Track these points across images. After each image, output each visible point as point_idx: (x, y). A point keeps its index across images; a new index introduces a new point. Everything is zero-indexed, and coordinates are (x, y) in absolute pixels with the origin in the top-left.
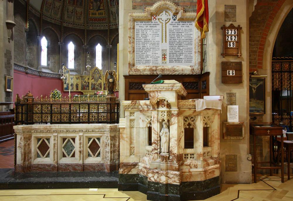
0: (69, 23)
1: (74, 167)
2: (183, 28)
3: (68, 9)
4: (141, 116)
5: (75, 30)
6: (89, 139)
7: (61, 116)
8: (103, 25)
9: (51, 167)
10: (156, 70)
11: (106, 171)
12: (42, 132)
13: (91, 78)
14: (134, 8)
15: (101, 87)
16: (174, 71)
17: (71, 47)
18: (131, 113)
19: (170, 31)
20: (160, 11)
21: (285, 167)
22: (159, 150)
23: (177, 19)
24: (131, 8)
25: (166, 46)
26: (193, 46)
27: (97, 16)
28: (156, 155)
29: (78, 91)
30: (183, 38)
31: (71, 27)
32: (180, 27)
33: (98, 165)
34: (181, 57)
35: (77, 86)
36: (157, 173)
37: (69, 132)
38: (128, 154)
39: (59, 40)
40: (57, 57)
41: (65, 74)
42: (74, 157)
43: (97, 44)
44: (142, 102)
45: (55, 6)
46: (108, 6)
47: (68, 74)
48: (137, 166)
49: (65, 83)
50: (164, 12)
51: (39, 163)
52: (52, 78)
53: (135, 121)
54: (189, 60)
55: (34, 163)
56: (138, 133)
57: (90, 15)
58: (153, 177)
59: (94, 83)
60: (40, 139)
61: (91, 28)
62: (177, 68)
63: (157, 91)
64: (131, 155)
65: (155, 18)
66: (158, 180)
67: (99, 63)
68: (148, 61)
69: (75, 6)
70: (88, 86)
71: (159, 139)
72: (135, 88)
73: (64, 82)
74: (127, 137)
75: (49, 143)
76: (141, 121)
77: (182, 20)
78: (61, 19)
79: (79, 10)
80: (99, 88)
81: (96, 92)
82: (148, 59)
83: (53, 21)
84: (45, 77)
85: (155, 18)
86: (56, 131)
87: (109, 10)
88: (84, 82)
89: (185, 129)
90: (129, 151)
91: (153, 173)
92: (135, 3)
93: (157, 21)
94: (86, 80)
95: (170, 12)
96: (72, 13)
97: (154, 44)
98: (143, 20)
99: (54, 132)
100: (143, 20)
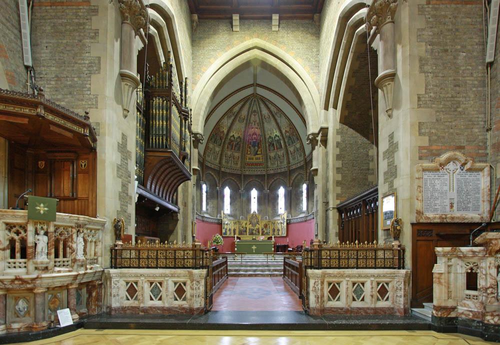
0: (227, 168)
1: (365, 310)
2: (471, 178)
3: (291, 151)
4: (460, 262)
5: (233, 175)
6: (378, 284)
9: (344, 310)
10: (446, 218)
11: (398, 314)
12: (335, 276)
13: (248, 223)
14: (420, 158)
15: (259, 232)
16: (464, 219)
17: (227, 191)
18: (448, 259)
19: (458, 180)
20: (448, 161)
22: (496, 294)
23: (465, 169)
25: (454, 194)
26: (481, 195)
30: (471, 187)
32: (467, 177)
33: (389, 309)
34: (469, 205)
35: (234, 231)
37: (174, 276)
38: (447, 299)
39: (218, 185)
40: (215, 202)
46: (266, 151)
48: (456, 310)
50: (452, 163)
51: (332, 307)
52: (212, 223)
54: (476, 208)
55: (327, 306)
56: (456, 279)
58: (493, 319)
60: (153, 283)
61: (247, 173)
62: (467, 216)
65: (443, 168)
67: (254, 207)
68: (436, 210)
69: (233, 151)
70: (246, 231)
71: (496, 283)
75: (339, 287)
76: (458, 267)
77: (470, 170)
79: (236, 155)
80: (257, 233)
81: (254, 237)
82: (436, 207)
83: (213, 166)
84: (207, 222)
85: (443, 168)
89: (467, 273)
90: (447, 295)
91: (492, 315)
94: (244, 225)
96: (230, 158)
97: (442, 193)
98: (432, 170)
99: (346, 277)
100: (432, 170)
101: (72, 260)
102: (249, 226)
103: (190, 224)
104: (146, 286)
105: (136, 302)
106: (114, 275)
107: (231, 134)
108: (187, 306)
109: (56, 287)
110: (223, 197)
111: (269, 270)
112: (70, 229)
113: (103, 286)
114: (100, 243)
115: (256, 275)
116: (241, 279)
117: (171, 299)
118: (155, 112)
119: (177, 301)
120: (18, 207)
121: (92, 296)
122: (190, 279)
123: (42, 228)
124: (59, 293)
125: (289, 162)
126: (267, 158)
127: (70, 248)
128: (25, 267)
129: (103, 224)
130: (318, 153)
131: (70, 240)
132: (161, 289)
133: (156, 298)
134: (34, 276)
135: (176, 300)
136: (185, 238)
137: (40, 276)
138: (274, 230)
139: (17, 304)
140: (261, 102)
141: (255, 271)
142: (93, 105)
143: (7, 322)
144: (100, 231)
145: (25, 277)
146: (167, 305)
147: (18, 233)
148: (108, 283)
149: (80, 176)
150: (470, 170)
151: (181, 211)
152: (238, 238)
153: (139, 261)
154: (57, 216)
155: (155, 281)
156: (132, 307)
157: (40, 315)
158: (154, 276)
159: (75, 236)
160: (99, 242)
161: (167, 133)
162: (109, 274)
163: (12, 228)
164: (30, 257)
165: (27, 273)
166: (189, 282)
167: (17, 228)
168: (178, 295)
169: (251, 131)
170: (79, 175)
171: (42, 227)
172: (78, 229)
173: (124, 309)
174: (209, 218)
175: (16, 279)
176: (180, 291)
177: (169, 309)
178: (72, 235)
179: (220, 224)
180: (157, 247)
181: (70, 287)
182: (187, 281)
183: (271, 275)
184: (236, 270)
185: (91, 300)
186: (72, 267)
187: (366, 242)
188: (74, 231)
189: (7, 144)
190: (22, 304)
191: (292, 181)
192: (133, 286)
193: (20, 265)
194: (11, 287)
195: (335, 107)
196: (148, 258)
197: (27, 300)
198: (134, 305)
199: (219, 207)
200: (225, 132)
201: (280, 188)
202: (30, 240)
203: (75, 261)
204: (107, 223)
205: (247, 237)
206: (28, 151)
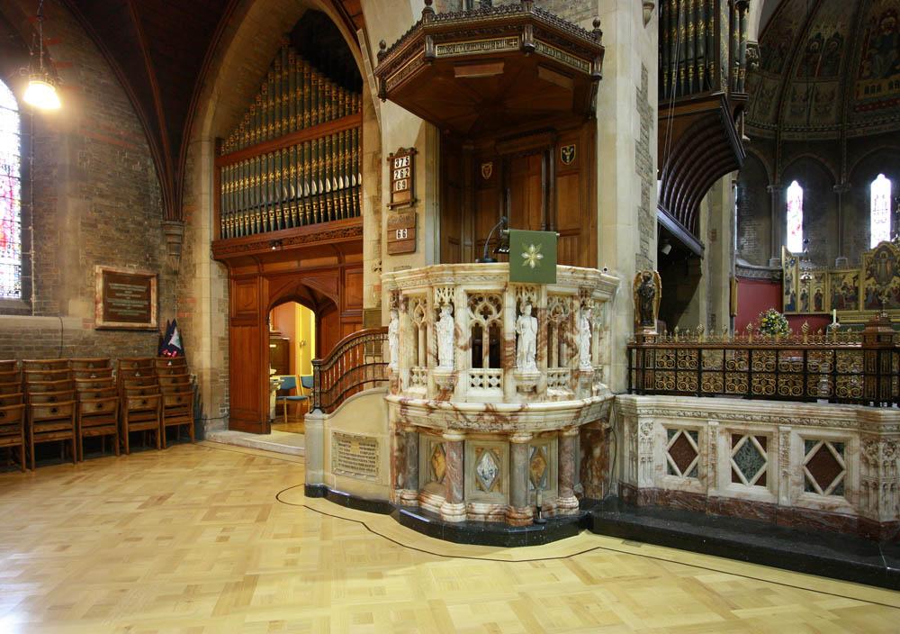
0: (796, 130)
3: (794, 93)
7: (777, 380)
8: (886, 118)
13: (863, 275)
17: (795, 193)
21: (32, 394)
29: (820, 313)
31: (800, 139)
39: (771, 178)
41: (787, 267)
42: (733, 481)
45: (764, 92)
47: (794, 268)
49: (788, 293)
52: (755, 281)
57: (858, 95)
60: (741, 437)
61: (860, 133)
70: (855, 299)
73: (785, 291)
78: (777, 122)
79: (825, 88)
88: (839, 289)
89: (830, 402)
94: (849, 280)
96: (805, 100)
101: (572, 370)
102: (866, 284)
103: (726, 283)
104: (723, 442)
105: (696, 482)
106: (643, 411)
107: (812, 34)
108: (852, 512)
109: (544, 432)
110: (783, 209)
112: (568, 301)
113: (612, 433)
114: (608, 332)
117: (798, 484)
118: (675, 7)
119: (812, 495)
120: (487, 257)
121: (592, 457)
122: (861, 434)
123: (529, 302)
124: (544, 445)
127: (569, 345)
128: (498, 385)
129: (612, 288)
131: (569, 326)
132: (764, 454)
133: (749, 478)
134: (517, 406)
135: (810, 488)
136: (713, 320)
137: (526, 407)
139: (478, 462)
142: (588, 10)
143: (466, 499)
144: (607, 304)
145: (502, 407)
146: (785, 501)
147: (486, 313)
148: (626, 428)
149: (562, 183)
151: (706, 253)
153: (700, 378)
154: (558, 273)
155: (746, 432)
156: (684, 492)
157: (521, 492)
158: (747, 419)
159: (577, 315)
160: (606, 329)
161: (707, 51)
162: (632, 406)
163: (476, 302)
164: (510, 364)
165: (505, 400)
166: (856, 443)
167: (486, 302)
168: (816, 479)
170: (559, 179)
171: (529, 298)
172: (582, 300)
173: (663, 495)
174: (748, 268)
175: (487, 411)
176: (824, 466)
177: (794, 515)
178: (572, 315)
179: (777, 281)
180: (750, 340)
181: (566, 434)
182: (848, 440)
185: (591, 466)
186: (573, 388)
187: (820, 331)
188: (577, 304)
189: (438, 134)
190: (487, 465)
192: (828, 450)
193: (491, 381)
194: (475, 426)
196: (724, 371)
197: (496, 456)
198: (688, 489)
199: (776, 235)
200: (795, 30)
201: (875, 178)
202: (509, 327)
203: (577, 374)
204: (621, 284)
206: (465, 147)
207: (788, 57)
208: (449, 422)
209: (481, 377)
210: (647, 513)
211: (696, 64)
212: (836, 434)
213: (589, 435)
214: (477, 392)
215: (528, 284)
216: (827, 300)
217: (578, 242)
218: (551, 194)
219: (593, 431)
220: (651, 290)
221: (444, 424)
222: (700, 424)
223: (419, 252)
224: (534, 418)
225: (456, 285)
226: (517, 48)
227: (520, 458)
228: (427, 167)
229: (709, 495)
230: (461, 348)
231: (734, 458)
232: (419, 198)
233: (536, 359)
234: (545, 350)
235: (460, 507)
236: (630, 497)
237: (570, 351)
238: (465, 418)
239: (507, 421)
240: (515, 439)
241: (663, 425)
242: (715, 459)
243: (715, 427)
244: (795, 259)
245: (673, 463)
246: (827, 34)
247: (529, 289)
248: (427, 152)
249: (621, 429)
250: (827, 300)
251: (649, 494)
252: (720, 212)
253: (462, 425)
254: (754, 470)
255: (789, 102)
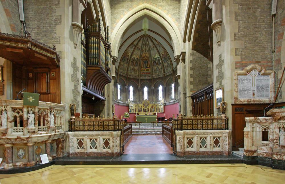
1: (207, 152)
4: (259, 125)
10: (251, 101)
12: (190, 134)
13: (143, 106)
14: (236, 68)
15: (149, 111)
16: (261, 101)
17: (131, 88)
18: (252, 124)
19: (257, 80)
20: (251, 70)
22: (278, 143)
23: (261, 74)
24: (235, 68)
25: (255, 88)
26: (269, 88)
27: (146, 71)
28: (277, 146)
30: (264, 84)
33: (220, 152)
34: (263, 94)
36: (280, 155)
40: (125, 94)
43: (159, 86)
44: (261, 118)
46: (152, 66)
48: (257, 152)
50: (253, 70)
52: (125, 106)
53: (255, 128)
54: (267, 96)
56: (256, 134)
58: (277, 157)
59: (144, 108)
61: (142, 78)
62: (262, 100)
63: (281, 112)
64: (253, 146)
65: (248, 73)
66: (281, 159)
68: (245, 97)
72: (238, 111)
74: (251, 137)
75: (193, 140)
76: (258, 128)
77: (263, 74)
79: (136, 68)
80: (148, 111)
82: (245, 95)
83: (123, 75)
85: (248, 73)
86: (198, 134)
87: (152, 68)
89: (263, 132)
90: (252, 144)
91: (277, 155)
92: (237, 65)
93: (250, 75)
94: (140, 106)
95: (257, 70)
98: (242, 75)
100: (242, 75)
102: (143, 107)
103: (111, 106)
105: (83, 150)
107: (133, 57)
108: (111, 152)
109: (40, 142)
110: (129, 91)
111: (155, 131)
112: (46, 110)
114: (63, 118)
115: (147, 134)
116: (139, 137)
117: (102, 148)
119: (105, 149)
121: (59, 147)
122: (112, 137)
125: (164, 72)
126: (153, 70)
128: (23, 131)
129: (64, 107)
130: (180, 66)
131: (47, 116)
132: (96, 142)
134: (28, 136)
136: (109, 114)
137: (31, 136)
138: (157, 109)
139: (18, 152)
140: (148, 39)
141: (147, 132)
143: (13, 162)
145: (22, 137)
146: (99, 151)
147: (18, 113)
150: (263, 74)
152: (138, 114)
153: (84, 127)
154: (39, 103)
155: (203, 137)
156: (81, 152)
158: (92, 135)
161: (98, 57)
162: (68, 134)
164: (25, 126)
165: (24, 135)
167: (18, 110)
169: (144, 55)
171: (31, 110)
172: (50, 110)
173: (76, 154)
176: (106, 143)
178: (47, 114)
179: (128, 106)
181: (47, 142)
182: (110, 138)
183: (156, 134)
184: (136, 132)
185: (59, 149)
186: (48, 131)
188: (49, 111)
190: (21, 152)
191: (166, 82)
192: (107, 140)
194: (15, 142)
195: (189, 41)
198: (81, 152)
199: (127, 97)
200: (130, 55)
202: (25, 116)
203: (49, 128)
205: (142, 114)
207: (129, 60)
208: (6, 142)
209: (45, 128)
210: (72, 158)
211: (96, 59)
212: (108, 137)
213: (58, 142)
214: (14, 134)
215: (30, 106)
216: (137, 110)
217: (54, 97)
218: (49, 84)
219: (59, 141)
220: (73, 108)
221: (4, 143)
222: (84, 137)
223: (5, 95)
224: (34, 139)
225: (7, 105)
226: (26, 47)
227: (30, 149)
228: (7, 72)
229: (85, 152)
230: (9, 122)
231: (78, 144)
232: (4, 80)
233: (34, 125)
234: (37, 122)
235: (11, 164)
236: (69, 155)
237: (47, 122)
238: (11, 141)
239: (25, 140)
240: (28, 145)
241: (76, 138)
242: (87, 144)
243: (86, 138)
244: (131, 102)
245: (214, 145)
246: (136, 58)
247: (31, 107)
248: (7, 68)
249: (67, 140)
250: (137, 110)
251: (72, 154)
252: (110, 91)
253: (10, 143)
254: (95, 146)
255: (165, 68)
